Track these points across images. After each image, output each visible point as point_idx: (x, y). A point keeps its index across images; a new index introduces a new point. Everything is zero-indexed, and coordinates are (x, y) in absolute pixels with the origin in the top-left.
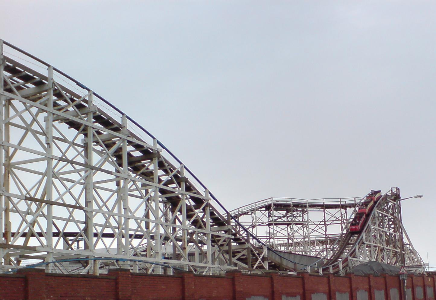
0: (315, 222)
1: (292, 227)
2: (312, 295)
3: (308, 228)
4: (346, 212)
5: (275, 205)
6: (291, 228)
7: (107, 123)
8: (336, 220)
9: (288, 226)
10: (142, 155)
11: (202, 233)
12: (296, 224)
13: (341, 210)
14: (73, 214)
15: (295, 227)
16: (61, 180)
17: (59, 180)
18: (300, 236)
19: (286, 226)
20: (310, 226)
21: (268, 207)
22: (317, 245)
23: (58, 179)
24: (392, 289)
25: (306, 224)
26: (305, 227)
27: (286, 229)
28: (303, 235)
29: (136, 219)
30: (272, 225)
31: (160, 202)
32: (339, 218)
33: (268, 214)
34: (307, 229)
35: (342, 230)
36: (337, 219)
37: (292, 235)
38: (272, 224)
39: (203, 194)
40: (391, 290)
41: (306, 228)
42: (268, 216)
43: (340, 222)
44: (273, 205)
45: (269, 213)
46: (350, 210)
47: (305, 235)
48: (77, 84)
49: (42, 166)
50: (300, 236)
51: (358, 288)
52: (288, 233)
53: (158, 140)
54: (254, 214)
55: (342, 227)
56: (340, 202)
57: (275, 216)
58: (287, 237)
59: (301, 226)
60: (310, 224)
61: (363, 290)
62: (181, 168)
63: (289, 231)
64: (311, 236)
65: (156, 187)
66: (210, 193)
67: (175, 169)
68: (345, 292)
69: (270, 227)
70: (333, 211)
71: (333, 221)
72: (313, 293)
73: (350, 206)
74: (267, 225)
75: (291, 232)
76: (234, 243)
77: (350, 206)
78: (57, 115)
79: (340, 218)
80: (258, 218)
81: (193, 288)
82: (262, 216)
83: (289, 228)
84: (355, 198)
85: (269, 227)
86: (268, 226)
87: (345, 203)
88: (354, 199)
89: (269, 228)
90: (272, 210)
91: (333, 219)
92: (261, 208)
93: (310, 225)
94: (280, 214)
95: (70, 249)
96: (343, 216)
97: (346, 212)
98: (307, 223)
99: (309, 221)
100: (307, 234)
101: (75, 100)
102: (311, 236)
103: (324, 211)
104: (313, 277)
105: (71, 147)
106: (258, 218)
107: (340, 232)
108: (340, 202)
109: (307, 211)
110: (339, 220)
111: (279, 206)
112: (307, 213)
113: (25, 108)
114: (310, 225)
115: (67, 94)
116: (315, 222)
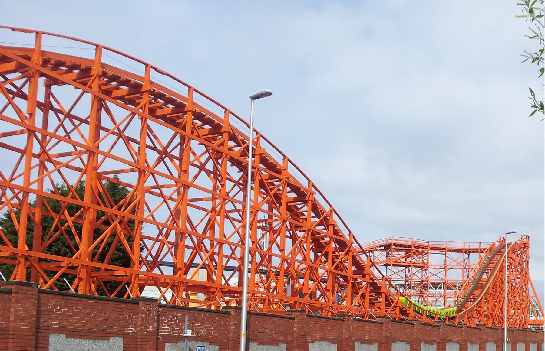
0: (435, 265)
1: (410, 270)
2: (447, 344)
3: (427, 272)
4: (469, 257)
5: (395, 245)
6: (409, 271)
7: (271, 166)
8: (456, 265)
9: (405, 268)
10: (297, 196)
11: (340, 275)
12: (415, 266)
13: (464, 255)
14: (158, 232)
15: (414, 270)
16: (55, 163)
17: (230, 220)
18: (418, 280)
19: (404, 268)
20: (430, 270)
21: (387, 247)
22: (429, 289)
23: (52, 162)
24: (519, 343)
25: (426, 267)
26: (424, 270)
27: (404, 271)
28: (421, 278)
29: (230, 244)
30: (391, 266)
31: (287, 237)
32: (461, 263)
33: (386, 254)
34: (426, 272)
35: (463, 277)
36: (459, 264)
37: (410, 278)
38: (390, 265)
39: (348, 237)
40: (517, 344)
41: (425, 271)
42: (386, 256)
43: (462, 267)
44: (393, 245)
45: (387, 253)
46: (475, 258)
47: (423, 278)
48: (155, 71)
49: (208, 205)
50: (418, 280)
51: (488, 340)
52: (406, 276)
53: (313, 182)
54: (372, 253)
55: (463, 273)
56: (464, 245)
57: (394, 256)
58: (404, 280)
59: (420, 268)
60: (430, 267)
61: (493, 343)
62: (331, 211)
63: (407, 273)
64: (430, 280)
65: (224, 199)
66: (354, 237)
67: (325, 211)
68: (475, 343)
69: (387, 267)
70: (454, 255)
71: (454, 266)
72: (448, 342)
73: (474, 251)
74: (384, 265)
75: (409, 274)
76: (92, 217)
77: (474, 251)
78: (76, 82)
79: (462, 263)
80: (375, 258)
81: (352, 330)
82: (380, 256)
83: (407, 270)
84: (480, 243)
85: (386, 267)
86: (385, 266)
87: (468, 247)
88: (478, 244)
89: (386, 268)
90: (391, 249)
91: (455, 263)
92: (380, 247)
93: (430, 268)
94: (399, 254)
95: (226, 285)
96: (466, 260)
97: (469, 257)
98: (427, 266)
99: (430, 264)
100: (425, 278)
101: (246, 143)
102: (430, 280)
103: (445, 254)
104: (449, 326)
105: (236, 186)
106: (375, 258)
107: (462, 279)
108: (464, 245)
109: (427, 253)
110: (461, 265)
111: (399, 247)
112: (427, 255)
113: (206, 150)
114: (430, 268)
115: (239, 136)
116: (435, 265)
